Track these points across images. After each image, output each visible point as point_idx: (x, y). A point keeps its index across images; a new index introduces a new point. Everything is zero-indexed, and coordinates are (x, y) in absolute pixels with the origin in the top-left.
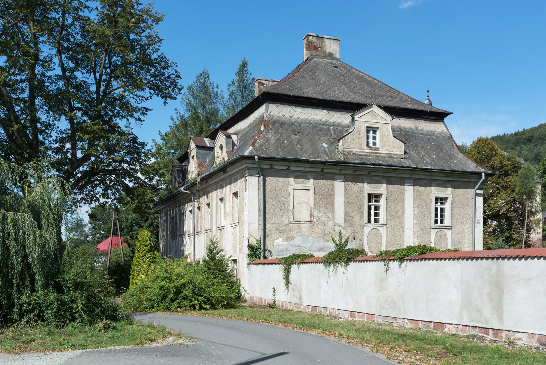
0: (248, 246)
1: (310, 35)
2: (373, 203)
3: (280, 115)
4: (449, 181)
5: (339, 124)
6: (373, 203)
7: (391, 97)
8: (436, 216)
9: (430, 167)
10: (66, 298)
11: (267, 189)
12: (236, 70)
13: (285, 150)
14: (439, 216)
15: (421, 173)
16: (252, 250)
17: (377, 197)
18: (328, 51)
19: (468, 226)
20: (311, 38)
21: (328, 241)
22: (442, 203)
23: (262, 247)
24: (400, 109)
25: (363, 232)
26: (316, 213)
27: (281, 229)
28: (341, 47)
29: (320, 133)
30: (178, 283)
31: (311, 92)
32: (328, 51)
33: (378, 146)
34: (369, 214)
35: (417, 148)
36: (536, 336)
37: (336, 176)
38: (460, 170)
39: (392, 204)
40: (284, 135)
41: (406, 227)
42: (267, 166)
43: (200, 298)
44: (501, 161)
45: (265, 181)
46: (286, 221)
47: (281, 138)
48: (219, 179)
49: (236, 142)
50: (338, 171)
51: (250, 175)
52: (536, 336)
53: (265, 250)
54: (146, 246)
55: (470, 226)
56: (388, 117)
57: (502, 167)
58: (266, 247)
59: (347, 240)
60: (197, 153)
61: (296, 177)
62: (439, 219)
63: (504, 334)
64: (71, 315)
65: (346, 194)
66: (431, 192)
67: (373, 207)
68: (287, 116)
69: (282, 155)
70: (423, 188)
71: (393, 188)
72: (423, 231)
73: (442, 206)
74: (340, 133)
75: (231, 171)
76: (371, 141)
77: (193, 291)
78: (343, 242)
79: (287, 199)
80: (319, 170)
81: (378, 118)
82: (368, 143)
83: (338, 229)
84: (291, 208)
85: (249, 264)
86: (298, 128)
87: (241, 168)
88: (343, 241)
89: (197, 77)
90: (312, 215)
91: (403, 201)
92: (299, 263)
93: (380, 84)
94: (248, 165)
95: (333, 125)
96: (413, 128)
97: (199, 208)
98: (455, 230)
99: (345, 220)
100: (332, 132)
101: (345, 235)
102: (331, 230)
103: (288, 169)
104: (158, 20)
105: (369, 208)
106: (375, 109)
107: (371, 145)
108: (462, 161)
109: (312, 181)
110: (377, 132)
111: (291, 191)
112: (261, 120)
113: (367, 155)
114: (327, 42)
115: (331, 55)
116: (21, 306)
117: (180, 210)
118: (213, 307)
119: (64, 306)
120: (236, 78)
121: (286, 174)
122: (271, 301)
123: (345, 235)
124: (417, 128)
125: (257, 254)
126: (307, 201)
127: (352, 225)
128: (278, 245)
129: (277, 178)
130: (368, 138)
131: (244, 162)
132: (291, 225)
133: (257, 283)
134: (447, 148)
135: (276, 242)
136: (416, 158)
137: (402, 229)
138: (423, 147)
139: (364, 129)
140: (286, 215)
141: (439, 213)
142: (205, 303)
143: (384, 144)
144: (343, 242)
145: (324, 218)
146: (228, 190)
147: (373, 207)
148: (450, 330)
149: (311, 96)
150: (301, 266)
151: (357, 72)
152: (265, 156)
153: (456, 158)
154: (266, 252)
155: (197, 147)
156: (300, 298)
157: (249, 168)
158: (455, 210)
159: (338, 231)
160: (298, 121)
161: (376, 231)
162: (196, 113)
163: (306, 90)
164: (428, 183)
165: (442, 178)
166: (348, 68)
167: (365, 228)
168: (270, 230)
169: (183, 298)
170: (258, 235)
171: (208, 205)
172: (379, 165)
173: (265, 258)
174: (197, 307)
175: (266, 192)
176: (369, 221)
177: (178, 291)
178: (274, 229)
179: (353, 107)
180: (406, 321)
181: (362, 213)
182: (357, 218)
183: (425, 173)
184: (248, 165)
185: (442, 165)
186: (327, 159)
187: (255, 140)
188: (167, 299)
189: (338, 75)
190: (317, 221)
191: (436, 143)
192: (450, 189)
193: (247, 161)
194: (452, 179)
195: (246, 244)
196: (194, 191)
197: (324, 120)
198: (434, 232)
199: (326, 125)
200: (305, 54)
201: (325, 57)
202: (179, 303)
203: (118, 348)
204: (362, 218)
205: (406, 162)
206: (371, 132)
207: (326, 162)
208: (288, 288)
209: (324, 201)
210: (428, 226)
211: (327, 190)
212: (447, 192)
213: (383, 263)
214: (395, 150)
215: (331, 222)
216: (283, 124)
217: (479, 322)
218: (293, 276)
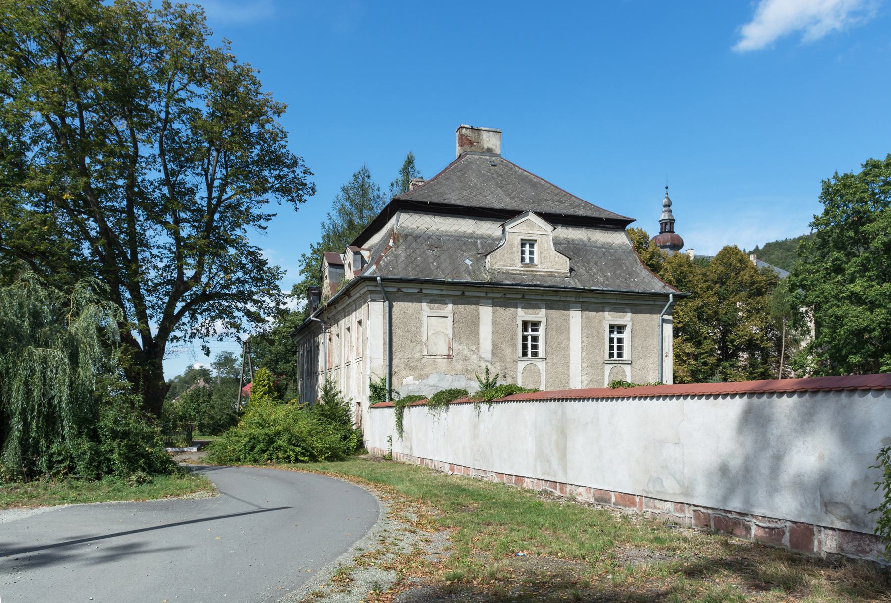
0: (370, 386)
1: (463, 127)
2: (530, 333)
3: (414, 226)
4: (627, 305)
5: (489, 236)
6: (530, 333)
7: (559, 201)
8: (611, 347)
9: (601, 288)
10: (103, 448)
11: (394, 316)
12: (401, 165)
13: (417, 269)
14: (616, 350)
15: (589, 295)
16: (375, 391)
17: (535, 325)
18: (485, 146)
19: (655, 358)
20: (464, 130)
21: (471, 380)
22: (619, 332)
23: (387, 388)
24: (567, 216)
25: (516, 368)
26: (456, 346)
27: (412, 365)
28: (501, 139)
29: (464, 248)
30: (274, 429)
31: (454, 198)
32: (485, 146)
33: (535, 262)
34: (525, 346)
35: (588, 263)
36: (592, 490)
37: (482, 300)
38: (641, 290)
39: (554, 333)
40: (417, 251)
41: (571, 362)
42: (393, 289)
43: (297, 448)
44: (752, 276)
45: (391, 308)
46: (418, 356)
47: (414, 255)
48: (345, 305)
49: (367, 260)
50: (483, 294)
51: (373, 300)
52: (592, 490)
53: (390, 391)
54: (264, 386)
55: (656, 360)
56: (548, 227)
57: (753, 283)
58: (393, 387)
59: (496, 378)
60: (330, 272)
61: (431, 302)
62: (615, 351)
63: (568, 488)
64: (108, 467)
65: (494, 322)
66: (604, 318)
67: (529, 338)
68: (423, 227)
69: (412, 275)
70: (594, 314)
71: (554, 313)
72: (593, 367)
73: (620, 336)
74: (490, 246)
75: (356, 294)
76: (527, 256)
77: (289, 440)
78: (490, 381)
79: (419, 328)
80: (460, 293)
81: (536, 228)
82: (523, 260)
83: (483, 365)
84: (424, 339)
85: (371, 408)
86: (435, 242)
87: (362, 292)
88: (491, 380)
89: (355, 176)
90: (451, 348)
91: (568, 329)
92: (411, 407)
93: (548, 185)
94: (370, 288)
95: (481, 237)
96: (585, 239)
97: (330, 339)
98: (637, 365)
99: (492, 353)
100: (479, 246)
101: (493, 371)
102: (475, 367)
103: (420, 292)
104: (279, 112)
105: (525, 338)
106: (532, 217)
107: (527, 261)
108: (647, 280)
109: (450, 306)
110: (535, 246)
111: (424, 319)
112: (391, 234)
113: (521, 274)
114: (485, 135)
115: (489, 151)
116: (51, 456)
117: (315, 341)
118: (314, 459)
119: (99, 456)
120: (400, 177)
121: (417, 298)
122: (386, 453)
123: (493, 371)
124: (589, 239)
125: (380, 394)
126: (444, 330)
127: (502, 359)
128: (408, 385)
129: (406, 304)
130: (523, 252)
131: (364, 284)
132: (424, 361)
133: (377, 428)
134: (627, 264)
135: (405, 381)
136: (586, 276)
137: (567, 365)
138: (596, 263)
139: (517, 242)
140: (418, 348)
141: (615, 344)
142: (303, 454)
143: (543, 259)
144: (490, 381)
145: (466, 352)
146: (354, 318)
147: (529, 338)
148: (527, 484)
149: (453, 203)
150: (412, 409)
151: (520, 171)
152: (390, 276)
153: (638, 276)
154: (393, 394)
155: (330, 264)
156: (411, 449)
157: (371, 292)
158: (636, 340)
159: (484, 367)
160: (437, 233)
161: (532, 367)
162: (351, 222)
163: (448, 196)
164: (600, 307)
165: (619, 301)
166: (510, 167)
167: (519, 363)
168: (398, 366)
169: (277, 449)
170: (383, 373)
171: (338, 335)
172: (535, 286)
173: (391, 399)
174: (292, 459)
175: (393, 320)
176: (525, 354)
177: (271, 441)
178: (403, 365)
179: (505, 215)
180: (494, 474)
181: (514, 345)
182: (508, 351)
183: (596, 295)
184: (370, 288)
185: (619, 285)
186: (469, 279)
187: (381, 257)
188: (256, 450)
189: (495, 176)
190: (458, 355)
191: (613, 258)
192: (629, 315)
193: (368, 283)
194: (627, 302)
195: (368, 383)
196: (325, 319)
197: (469, 231)
198: (608, 368)
199: (472, 237)
200: (458, 150)
201: (483, 153)
202: (271, 455)
203: (114, 502)
204: (514, 351)
205: (571, 281)
206: (527, 246)
207: (467, 283)
208: (401, 436)
209: (467, 330)
210: (600, 361)
211: (469, 317)
212: (626, 319)
213: (472, 406)
214: (557, 266)
215: (475, 357)
216: (417, 237)
217: (549, 474)
218: (405, 421)
